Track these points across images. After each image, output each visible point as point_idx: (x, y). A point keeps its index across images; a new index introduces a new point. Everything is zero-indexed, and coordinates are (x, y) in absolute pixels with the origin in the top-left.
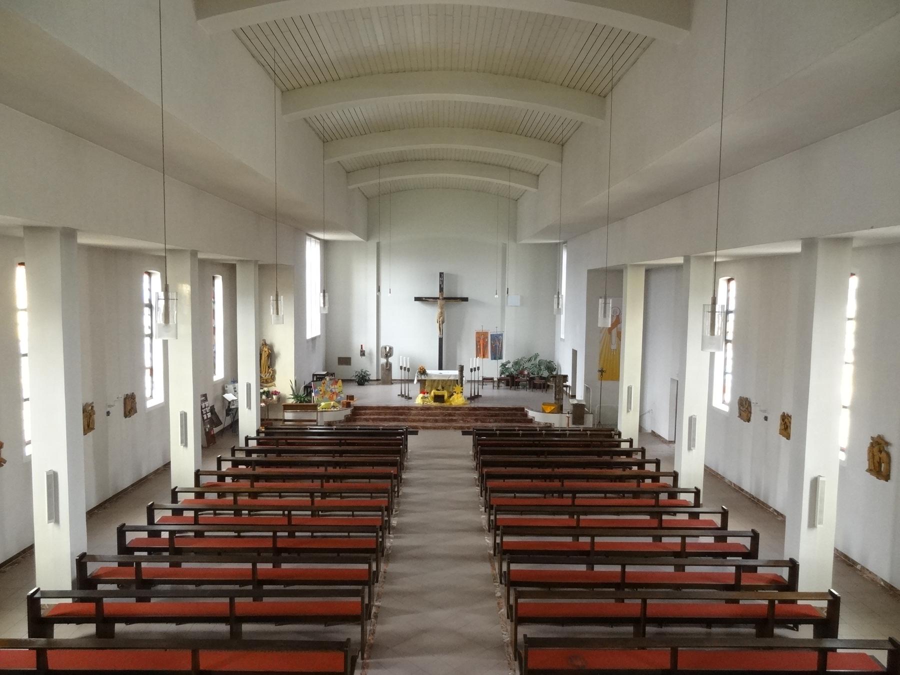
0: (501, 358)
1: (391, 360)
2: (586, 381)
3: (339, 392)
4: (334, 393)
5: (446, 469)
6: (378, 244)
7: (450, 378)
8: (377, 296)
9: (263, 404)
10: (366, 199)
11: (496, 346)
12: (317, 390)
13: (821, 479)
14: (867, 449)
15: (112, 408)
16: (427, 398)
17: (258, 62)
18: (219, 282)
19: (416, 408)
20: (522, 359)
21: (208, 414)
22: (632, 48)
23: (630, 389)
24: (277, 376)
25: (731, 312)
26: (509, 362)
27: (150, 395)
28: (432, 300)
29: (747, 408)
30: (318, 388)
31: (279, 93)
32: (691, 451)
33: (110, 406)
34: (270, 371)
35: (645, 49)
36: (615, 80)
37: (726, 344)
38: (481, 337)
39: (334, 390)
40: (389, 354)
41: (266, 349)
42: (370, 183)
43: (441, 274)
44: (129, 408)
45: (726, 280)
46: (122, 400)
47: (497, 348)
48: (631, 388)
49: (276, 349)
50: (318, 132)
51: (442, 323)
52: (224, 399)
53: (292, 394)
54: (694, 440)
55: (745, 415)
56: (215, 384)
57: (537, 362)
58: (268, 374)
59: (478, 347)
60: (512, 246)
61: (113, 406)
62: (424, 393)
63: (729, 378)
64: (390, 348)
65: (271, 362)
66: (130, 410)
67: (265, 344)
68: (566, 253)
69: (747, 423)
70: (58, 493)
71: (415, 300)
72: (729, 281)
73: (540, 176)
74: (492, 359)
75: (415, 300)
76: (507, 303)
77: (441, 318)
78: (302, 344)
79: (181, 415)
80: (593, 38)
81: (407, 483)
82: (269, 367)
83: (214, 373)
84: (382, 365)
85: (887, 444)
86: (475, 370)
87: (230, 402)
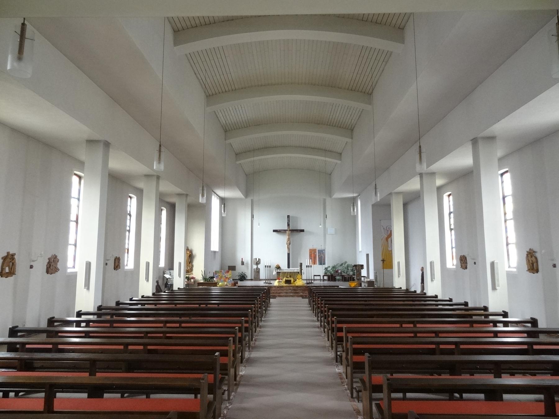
0: (324, 264)
1: (259, 266)
2: (375, 269)
3: (230, 278)
4: (226, 278)
7: (294, 271)
10: (245, 175)
11: (321, 257)
12: (217, 275)
13: (495, 262)
14: (525, 259)
15: (109, 261)
16: (281, 282)
18: (164, 213)
19: (275, 287)
20: (337, 265)
23: (399, 263)
24: (194, 268)
25: (452, 212)
26: (329, 267)
29: (465, 261)
30: (218, 274)
31: (206, 97)
34: (190, 265)
35: (387, 62)
37: (451, 231)
39: (226, 276)
40: (258, 263)
41: (189, 252)
42: (247, 162)
43: (288, 216)
44: (117, 265)
45: (447, 195)
46: (114, 259)
47: (322, 258)
49: (194, 253)
51: (289, 244)
52: (164, 276)
54: (434, 275)
57: (346, 266)
60: (328, 201)
61: (36, 261)
62: (279, 279)
64: (259, 259)
65: (191, 260)
68: (360, 202)
69: (466, 270)
70: (91, 266)
72: (449, 195)
73: (342, 154)
74: (319, 265)
77: (289, 241)
78: (209, 254)
81: (269, 310)
82: (189, 263)
84: (254, 269)
85: (534, 252)
86: (309, 267)
87: (167, 279)
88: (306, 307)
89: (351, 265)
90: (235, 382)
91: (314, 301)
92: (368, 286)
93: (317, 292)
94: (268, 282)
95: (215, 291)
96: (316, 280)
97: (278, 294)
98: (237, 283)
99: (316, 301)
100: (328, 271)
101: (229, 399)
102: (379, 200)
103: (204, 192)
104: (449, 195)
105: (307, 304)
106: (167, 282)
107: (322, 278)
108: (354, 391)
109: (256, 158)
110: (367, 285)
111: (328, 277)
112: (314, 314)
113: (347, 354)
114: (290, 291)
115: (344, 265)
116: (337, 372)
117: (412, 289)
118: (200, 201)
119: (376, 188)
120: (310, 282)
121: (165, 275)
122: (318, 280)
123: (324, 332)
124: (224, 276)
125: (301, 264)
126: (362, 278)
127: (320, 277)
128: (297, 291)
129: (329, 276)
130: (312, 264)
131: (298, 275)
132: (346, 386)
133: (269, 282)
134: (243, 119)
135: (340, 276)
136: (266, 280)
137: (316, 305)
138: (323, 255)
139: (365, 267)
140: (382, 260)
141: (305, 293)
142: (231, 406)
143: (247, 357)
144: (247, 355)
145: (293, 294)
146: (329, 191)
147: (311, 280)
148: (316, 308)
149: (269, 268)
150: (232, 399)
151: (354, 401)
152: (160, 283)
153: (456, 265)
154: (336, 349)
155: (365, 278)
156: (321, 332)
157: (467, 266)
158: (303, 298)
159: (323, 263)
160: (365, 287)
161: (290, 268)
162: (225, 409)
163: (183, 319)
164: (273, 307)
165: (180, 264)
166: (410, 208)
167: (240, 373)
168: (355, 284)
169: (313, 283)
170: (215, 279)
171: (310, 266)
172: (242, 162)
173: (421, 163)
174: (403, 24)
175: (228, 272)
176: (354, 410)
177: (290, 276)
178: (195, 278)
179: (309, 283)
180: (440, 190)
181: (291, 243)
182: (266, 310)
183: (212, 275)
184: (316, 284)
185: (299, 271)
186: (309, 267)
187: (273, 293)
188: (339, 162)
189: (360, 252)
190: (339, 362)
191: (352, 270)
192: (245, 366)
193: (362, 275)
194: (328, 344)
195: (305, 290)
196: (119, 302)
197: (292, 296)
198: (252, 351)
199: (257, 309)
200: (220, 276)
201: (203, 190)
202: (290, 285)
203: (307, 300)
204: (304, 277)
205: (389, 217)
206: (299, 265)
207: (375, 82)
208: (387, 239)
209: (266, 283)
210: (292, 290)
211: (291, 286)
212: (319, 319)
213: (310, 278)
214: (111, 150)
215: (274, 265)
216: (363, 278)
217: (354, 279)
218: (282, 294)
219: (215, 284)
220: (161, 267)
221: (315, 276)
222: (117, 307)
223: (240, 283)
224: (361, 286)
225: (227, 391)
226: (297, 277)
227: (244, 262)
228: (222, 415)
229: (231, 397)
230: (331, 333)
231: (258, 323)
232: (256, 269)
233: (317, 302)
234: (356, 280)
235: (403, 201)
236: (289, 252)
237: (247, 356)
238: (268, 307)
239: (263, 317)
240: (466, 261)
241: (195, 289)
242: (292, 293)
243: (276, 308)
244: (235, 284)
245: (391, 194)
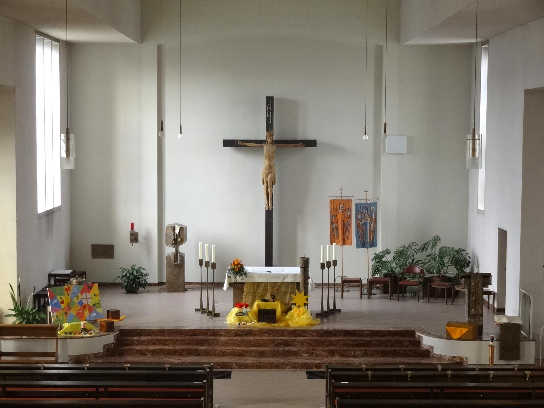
0: (373, 244)
1: (182, 249)
2: (523, 284)
3: (94, 305)
4: (85, 307)
6: (160, 49)
11: (365, 224)
12: (55, 301)
16: (246, 314)
19: (228, 332)
20: (410, 247)
26: (387, 252)
28: (253, 145)
30: (58, 297)
39: (85, 302)
40: (179, 239)
43: (270, 100)
57: (437, 252)
59: (334, 225)
62: (241, 307)
64: (182, 229)
74: (358, 247)
77: (270, 176)
84: (168, 258)
86: (329, 266)
89: (453, 248)
115: (432, 248)
124: (77, 301)
138: (371, 220)
149: (210, 268)
159: (368, 241)
177: (274, 297)
200: (65, 303)
232: (173, 257)
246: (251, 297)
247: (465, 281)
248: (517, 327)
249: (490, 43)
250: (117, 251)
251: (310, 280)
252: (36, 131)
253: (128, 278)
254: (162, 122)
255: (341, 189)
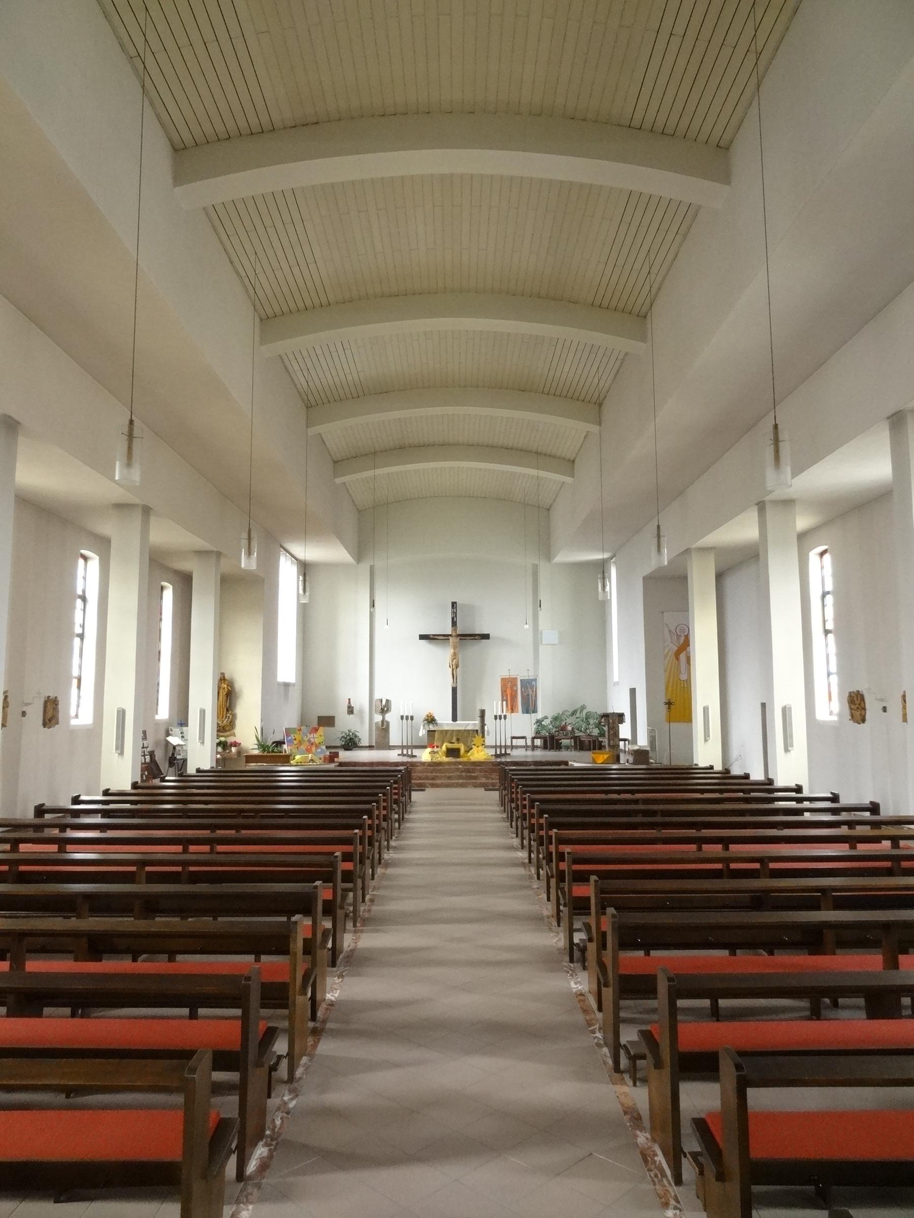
0: (535, 711)
1: (388, 717)
3: (320, 743)
4: (312, 744)
5: (470, 921)
8: (370, 612)
9: (219, 756)
11: (528, 695)
12: (290, 738)
16: (437, 752)
17: (238, 273)
18: (168, 595)
19: (423, 764)
20: (563, 713)
21: (146, 757)
22: (670, 236)
23: (706, 710)
24: (238, 723)
25: (828, 593)
26: (546, 718)
27: (75, 714)
28: (442, 638)
29: (859, 704)
31: (257, 320)
32: (788, 754)
33: (27, 704)
34: (228, 715)
35: (685, 236)
36: (653, 291)
37: (826, 635)
38: (508, 688)
39: (312, 740)
40: (386, 709)
41: (225, 686)
42: (356, 479)
43: (454, 605)
44: (50, 715)
48: (708, 708)
50: (301, 390)
51: (455, 667)
53: (256, 743)
55: (857, 714)
56: (157, 724)
57: (584, 716)
58: (226, 720)
60: (545, 570)
61: (30, 704)
62: (433, 747)
63: (834, 679)
64: (387, 701)
66: (51, 717)
67: (223, 679)
71: (420, 639)
72: (822, 554)
75: (420, 639)
76: (541, 640)
77: (455, 660)
79: (118, 711)
80: (624, 227)
81: (409, 821)
82: (227, 710)
83: (157, 712)
86: (500, 718)
87: (174, 747)
88: (494, 812)
90: (311, 1024)
91: (512, 801)
92: (635, 763)
93: (519, 780)
94: (407, 752)
95: (288, 774)
96: (517, 747)
97: (430, 781)
98: (337, 755)
99: (517, 799)
100: (544, 727)
101: (291, 1079)
102: (666, 563)
103: (252, 544)
104: (822, 554)
105: (498, 805)
106: (173, 754)
107: (529, 743)
108: (622, 1052)
109: (379, 472)
110: (631, 759)
111: (542, 740)
112: (514, 830)
113: (603, 946)
114: (458, 773)
115: (580, 713)
116: (574, 990)
117: (736, 771)
118: (243, 566)
119: (659, 536)
120: (503, 752)
121: (170, 739)
122: (521, 747)
123: (538, 878)
124: (307, 739)
125: (483, 713)
126: (621, 742)
127: (524, 740)
128: (473, 774)
129: (545, 739)
130: (507, 712)
131: (475, 737)
132: (599, 1035)
133: (410, 753)
134: (349, 378)
135: (572, 738)
136: (402, 747)
137: (517, 810)
139: (628, 718)
140: (667, 703)
141: (492, 779)
142: (294, 1102)
143: (350, 948)
144: (348, 941)
145: (465, 781)
146: (546, 549)
147: (506, 747)
148: (519, 817)
150: (300, 1079)
151: (622, 1080)
152: (159, 756)
153: (840, 715)
154: (571, 924)
155: (627, 742)
156: (531, 877)
157: (864, 716)
158: (485, 790)
159: (531, 708)
160: (628, 766)
161: (458, 722)
162: (276, 1111)
163: (220, 833)
164: (416, 812)
165: (203, 712)
166: (730, 582)
167: (329, 996)
168: (606, 756)
169: (509, 754)
170: (285, 746)
171: (503, 717)
172: (346, 479)
173: (779, 463)
174: (644, 310)
175: (316, 730)
176: (626, 1113)
178: (240, 744)
179: (501, 755)
180: (804, 539)
181: (460, 664)
182: (400, 821)
183: (279, 738)
184: (516, 757)
185: (478, 728)
186: (500, 719)
187: (420, 778)
188: (568, 480)
189: (614, 685)
190: (578, 962)
191: (598, 725)
192: (341, 976)
193: (621, 737)
194: (548, 909)
195: (493, 771)
196: (44, 808)
197: (462, 785)
198: (362, 931)
199: (377, 822)
201: (249, 539)
202: (458, 760)
203: (495, 795)
204: (490, 740)
205: (684, 607)
206: (478, 714)
207: (655, 286)
208: (677, 655)
209: (403, 755)
210: (462, 771)
211: (460, 763)
212: (526, 842)
213: (503, 744)
214: (21, 439)
215: (421, 715)
216: (622, 743)
217: (603, 744)
218: (438, 782)
219: (286, 759)
220: (160, 720)
221: (513, 738)
222: (38, 821)
223: (345, 756)
224: (617, 760)
225: (285, 1057)
226: (473, 741)
227: (353, 707)
228: (268, 1132)
229: (299, 1072)
230: (558, 887)
231: (380, 853)
232: (380, 723)
233: (519, 802)
234: (607, 747)
235: (716, 570)
236: (455, 685)
237: (349, 946)
238: (405, 811)
239: (394, 838)
240: (862, 704)
241: (236, 772)
242: (460, 777)
243: (427, 816)
244: (332, 758)
245: (687, 551)
246: (441, 742)
247: (605, 720)
248: (646, 752)
249: (617, 556)
250: (337, 722)
251: (486, 727)
252: (278, 589)
253: (346, 738)
254: (374, 601)
255: (509, 670)
